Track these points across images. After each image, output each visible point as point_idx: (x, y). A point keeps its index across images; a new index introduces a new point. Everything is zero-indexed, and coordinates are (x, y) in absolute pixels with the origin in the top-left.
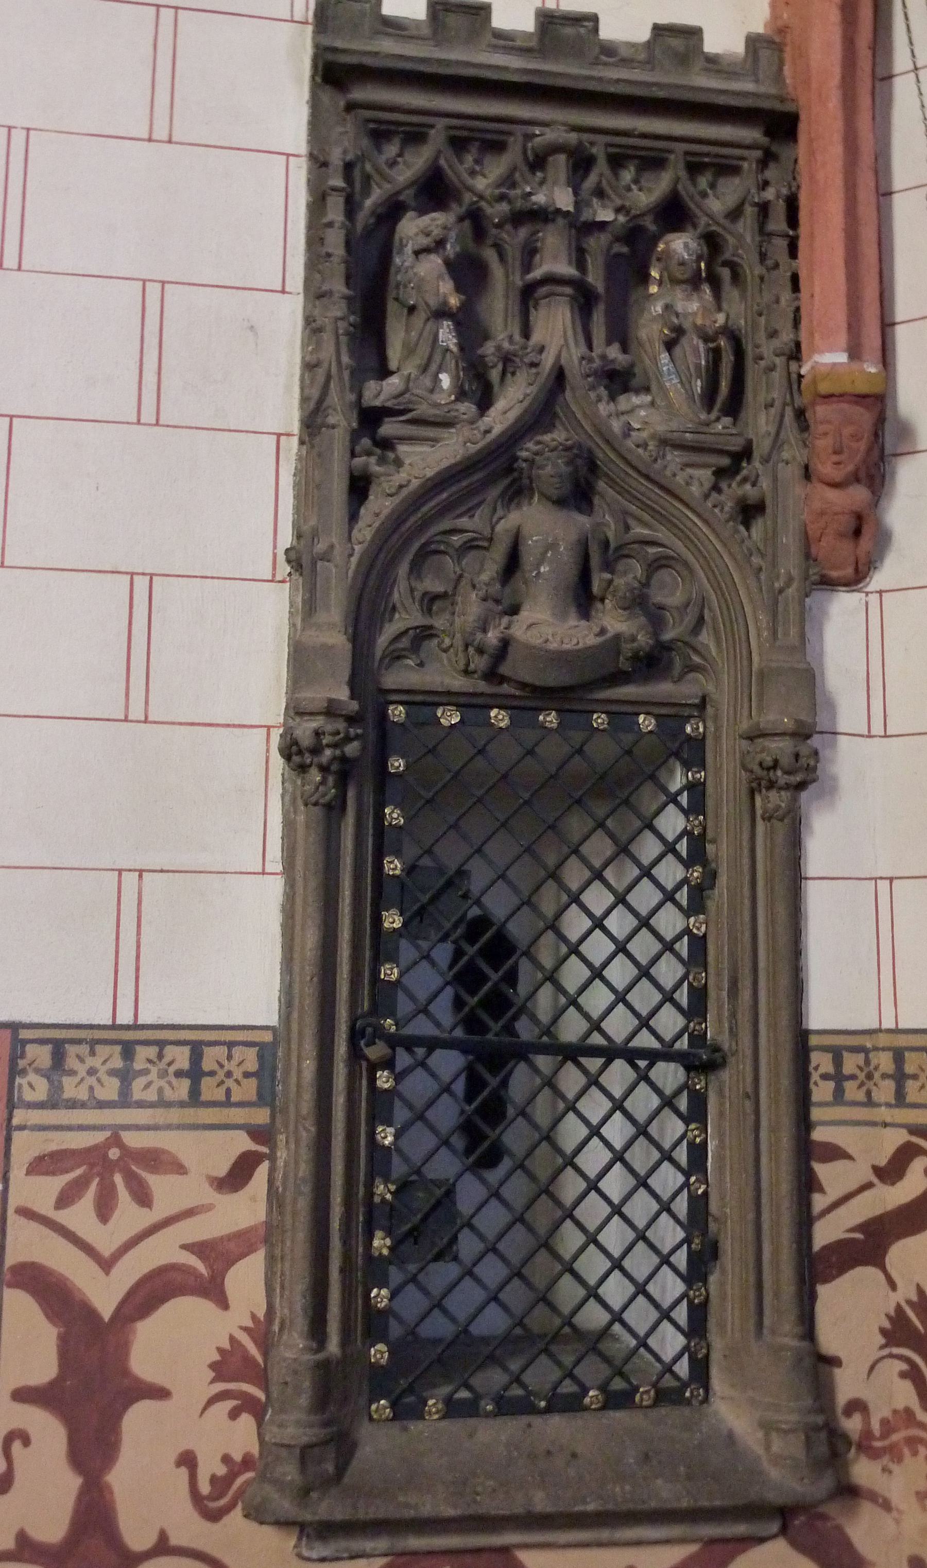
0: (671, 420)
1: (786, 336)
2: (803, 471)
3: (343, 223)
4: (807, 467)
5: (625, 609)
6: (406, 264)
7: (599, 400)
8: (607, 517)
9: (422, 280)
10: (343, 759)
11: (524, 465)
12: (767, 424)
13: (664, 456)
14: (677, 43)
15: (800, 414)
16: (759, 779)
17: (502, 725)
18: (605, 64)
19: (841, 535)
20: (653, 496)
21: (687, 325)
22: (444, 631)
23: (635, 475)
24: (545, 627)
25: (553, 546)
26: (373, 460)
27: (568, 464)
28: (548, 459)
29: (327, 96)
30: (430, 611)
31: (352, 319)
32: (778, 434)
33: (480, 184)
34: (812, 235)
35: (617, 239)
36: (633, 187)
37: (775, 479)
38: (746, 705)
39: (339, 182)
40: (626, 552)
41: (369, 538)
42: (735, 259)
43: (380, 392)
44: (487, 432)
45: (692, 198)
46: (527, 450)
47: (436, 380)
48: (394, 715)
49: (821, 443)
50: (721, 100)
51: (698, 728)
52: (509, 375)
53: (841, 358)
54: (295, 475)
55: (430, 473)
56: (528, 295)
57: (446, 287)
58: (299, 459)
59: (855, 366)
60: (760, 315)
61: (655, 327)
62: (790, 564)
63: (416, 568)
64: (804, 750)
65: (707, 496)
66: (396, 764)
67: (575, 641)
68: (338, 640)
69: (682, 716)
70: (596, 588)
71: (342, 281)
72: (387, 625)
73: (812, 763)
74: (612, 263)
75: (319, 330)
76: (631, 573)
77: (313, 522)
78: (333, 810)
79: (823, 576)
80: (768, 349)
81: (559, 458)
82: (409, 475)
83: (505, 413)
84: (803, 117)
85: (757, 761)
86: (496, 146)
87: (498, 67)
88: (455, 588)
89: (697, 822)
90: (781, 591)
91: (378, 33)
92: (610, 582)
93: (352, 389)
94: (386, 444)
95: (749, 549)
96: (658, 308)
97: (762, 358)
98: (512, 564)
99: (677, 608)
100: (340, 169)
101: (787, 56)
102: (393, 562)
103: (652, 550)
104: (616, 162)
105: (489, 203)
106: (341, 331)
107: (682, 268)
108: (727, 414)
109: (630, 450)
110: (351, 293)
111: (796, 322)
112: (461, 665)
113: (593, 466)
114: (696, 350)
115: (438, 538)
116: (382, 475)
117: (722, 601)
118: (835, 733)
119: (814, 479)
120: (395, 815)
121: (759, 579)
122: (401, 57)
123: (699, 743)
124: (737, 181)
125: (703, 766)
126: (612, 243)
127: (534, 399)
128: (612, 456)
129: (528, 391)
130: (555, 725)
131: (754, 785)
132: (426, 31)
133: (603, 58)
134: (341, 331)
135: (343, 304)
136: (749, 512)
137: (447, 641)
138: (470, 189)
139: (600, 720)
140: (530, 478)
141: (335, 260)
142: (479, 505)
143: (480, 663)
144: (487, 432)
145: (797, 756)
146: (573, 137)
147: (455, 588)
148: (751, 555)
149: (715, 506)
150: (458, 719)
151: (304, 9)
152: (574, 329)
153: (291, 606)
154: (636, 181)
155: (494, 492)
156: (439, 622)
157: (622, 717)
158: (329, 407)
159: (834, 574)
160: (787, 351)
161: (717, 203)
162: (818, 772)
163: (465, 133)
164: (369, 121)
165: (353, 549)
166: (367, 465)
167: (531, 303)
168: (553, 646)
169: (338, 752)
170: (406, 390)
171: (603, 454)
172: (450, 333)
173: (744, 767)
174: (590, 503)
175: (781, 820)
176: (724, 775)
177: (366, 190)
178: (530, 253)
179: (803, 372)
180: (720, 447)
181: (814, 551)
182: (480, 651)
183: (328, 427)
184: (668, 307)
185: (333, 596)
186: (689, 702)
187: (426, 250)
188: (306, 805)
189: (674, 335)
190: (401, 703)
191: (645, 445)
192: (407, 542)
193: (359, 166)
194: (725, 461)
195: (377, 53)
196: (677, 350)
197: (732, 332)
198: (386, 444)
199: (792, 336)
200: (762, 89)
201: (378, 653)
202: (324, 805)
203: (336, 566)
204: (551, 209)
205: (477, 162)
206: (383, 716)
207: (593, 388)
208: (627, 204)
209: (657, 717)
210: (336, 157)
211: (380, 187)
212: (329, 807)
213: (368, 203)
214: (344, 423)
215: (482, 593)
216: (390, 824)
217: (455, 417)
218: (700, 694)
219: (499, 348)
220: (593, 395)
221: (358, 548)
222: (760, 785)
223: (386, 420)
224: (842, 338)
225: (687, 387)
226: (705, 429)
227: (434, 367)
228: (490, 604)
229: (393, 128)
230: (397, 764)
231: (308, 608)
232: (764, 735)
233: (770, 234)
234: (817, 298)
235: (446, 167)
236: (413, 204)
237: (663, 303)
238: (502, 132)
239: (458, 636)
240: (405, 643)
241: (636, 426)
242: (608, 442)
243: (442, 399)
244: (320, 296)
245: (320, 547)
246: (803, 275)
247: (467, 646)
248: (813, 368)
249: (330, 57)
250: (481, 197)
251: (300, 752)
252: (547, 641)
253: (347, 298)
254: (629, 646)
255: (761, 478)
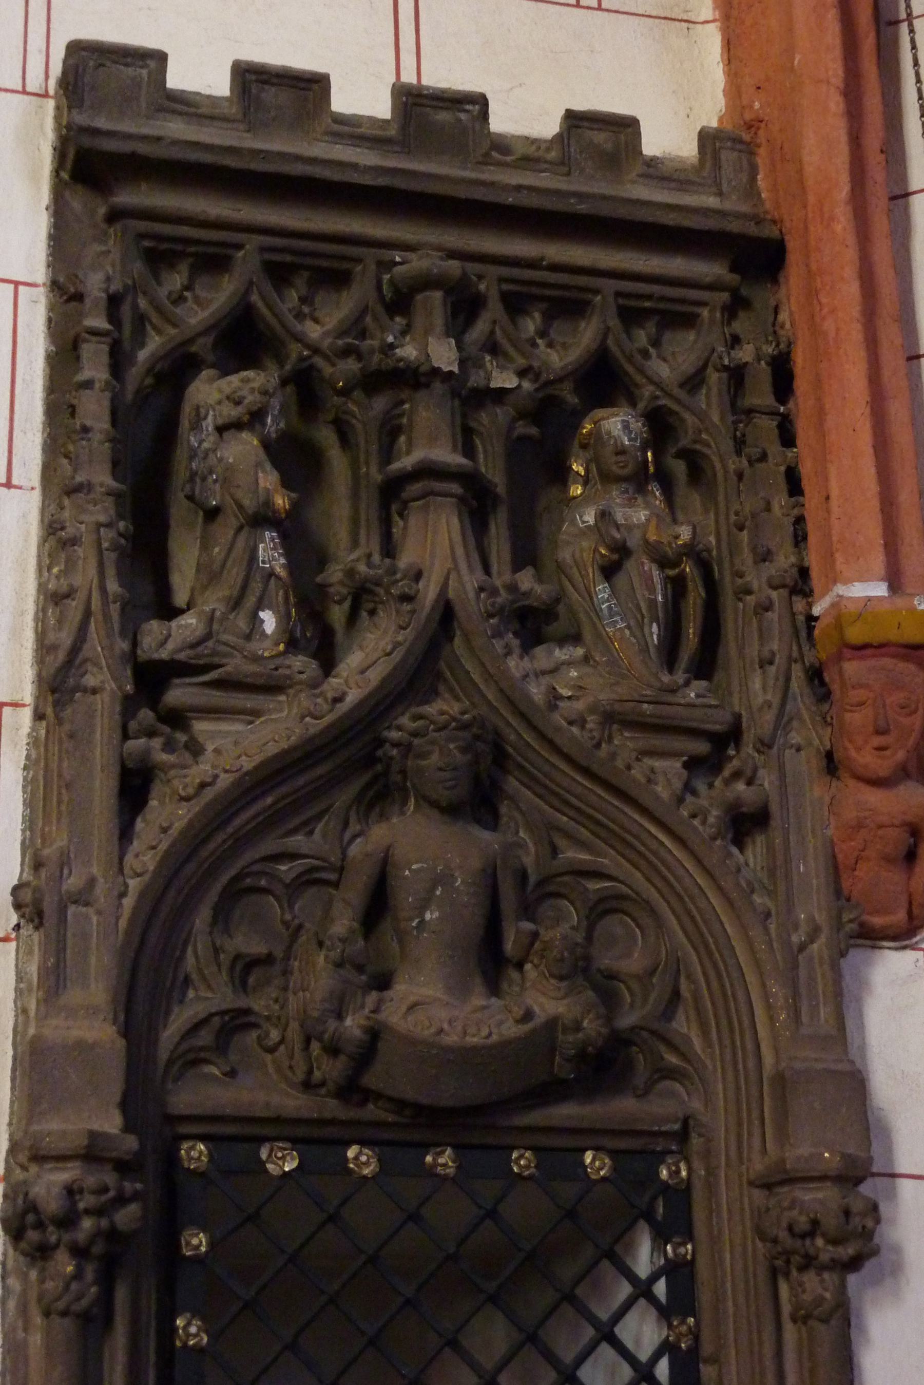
0: (617, 683)
1: (785, 560)
2: (824, 763)
3: (107, 383)
4: (829, 755)
5: (561, 978)
6: (206, 445)
7: (508, 653)
8: (522, 834)
9: (230, 468)
10: (112, 1235)
11: (395, 752)
12: (764, 688)
13: (610, 739)
14: (600, 137)
15: (815, 675)
16: (788, 1254)
17: (366, 1171)
18: (500, 164)
19: (888, 859)
20: (593, 799)
21: (633, 542)
22: (268, 1018)
23: (563, 766)
24: (432, 1006)
25: (444, 879)
26: (157, 743)
27: (464, 750)
28: (433, 743)
29: (77, 202)
30: (244, 983)
31: (122, 525)
32: (783, 704)
33: (313, 331)
34: (821, 413)
35: (522, 415)
36: (539, 341)
37: (782, 776)
38: (757, 1132)
39: (100, 322)
40: (551, 888)
41: (151, 868)
42: (698, 447)
43: (165, 639)
44: (338, 700)
45: (630, 359)
46: (399, 728)
47: (255, 621)
48: (191, 1159)
49: (856, 719)
50: (670, 219)
51: (678, 1172)
52: (364, 614)
53: (879, 590)
54: (25, 768)
55: (247, 764)
56: (393, 494)
57: (269, 479)
58: (34, 741)
59: (900, 602)
60: (741, 529)
61: (585, 544)
62: (812, 907)
63: (222, 916)
64: (857, 1206)
65: (680, 800)
66: (195, 1241)
67: (485, 1032)
68: (102, 1032)
69: (653, 1152)
70: (509, 947)
71: (108, 466)
72: (176, 1010)
73: (870, 1224)
74: (516, 449)
75: (74, 541)
76: (563, 925)
77: (61, 841)
78: (93, 1323)
79: (862, 925)
80: (756, 578)
81: (449, 740)
82: (214, 767)
83: (363, 672)
84: (793, 245)
85: (784, 1225)
86: (336, 278)
87: (341, 165)
88: (290, 947)
89: (684, 1329)
90: (802, 948)
91: (161, 109)
92: (535, 935)
93: (123, 634)
94: (177, 719)
95: (749, 883)
96: (590, 517)
97: (749, 592)
98: (378, 906)
99: (638, 977)
100: (103, 304)
101: (762, 159)
102: (184, 910)
103: (594, 885)
104: (515, 305)
105: (326, 358)
106: (105, 545)
107: (621, 458)
108: (698, 677)
109: (558, 729)
110: (122, 487)
111: (800, 538)
112: (300, 1076)
113: (500, 756)
114: (648, 581)
115: (256, 868)
116: (173, 766)
117: (708, 965)
118: (894, 1176)
119: (842, 773)
120: (193, 1330)
121: (766, 930)
122: (196, 145)
123: (680, 1196)
124: (692, 336)
125: (690, 1236)
126: (515, 420)
127: (408, 652)
128: (529, 737)
129: (400, 638)
130: (451, 1171)
131: (779, 1263)
132: (233, 110)
133: (494, 154)
134: (105, 545)
135: (109, 502)
136: (745, 823)
137: (275, 1035)
138: (298, 338)
139: (522, 1161)
140: (403, 772)
141: (97, 437)
142: (319, 817)
143: (331, 1070)
144: (338, 700)
145: (847, 1213)
146: (454, 267)
147: (290, 947)
148: (752, 892)
149: (694, 816)
150: (295, 1164)
151: (42, 76)
152: (465, 547)
153: (20, 978)
154: (543, 333)
155: (343, 797)
156: (259, 1004)
157: (558, 1157)
158: (85, 661)
159: (877, 921)
160: (789, 581)
161: (669, 363)
162: (876, 1240)
163: (288, 258)
164: (142, 236)
165: (126, 885)
166: (148, 751)
167: (394, 508)
168: (451, 1039)
169: (104, 1223)
170: (208, 636)
171: (517, 734)
172: (274, 549)
173: (761, 1234)
174: (496, 816)
175: (825, 1321)
176: (727, 1246)
177: (140, 338)
178: (391, 432)
179: (816, 611)
180: (695, 725)
181: (846, 885)
182: (333, 1050)
183: (85, 690)
184: (604, 515)
185: (93, 960)
186: (663, 1128)
187: (237, 426)
188: (47, 1314)
189: (615, 557)
190: (203, 1138)
191: (581, 722)
192: (212, 871)
193: (129, 299)
194: (702, 747)
195: (159, 139)
196: (621, 579)
197: (698, 554)
198: (177, 719)
199: (793, 559)
200: (728, 206)
201: (163, 1055)
202: (78, 1316)
203: (99, 913)
204: (423, 369)
205: (303, 300)
206: (171, 1160)
207: (498, 634)
208: (536, 364)
209: (614, 1154)
210: (95, 285)
211: (159, 332)
212: (85, 1318)
213: (143, 355)
214: (111, 685)
215: (335, 954)
216: (185, 1345)
217: (289, 677)
218: (681, 1115)
219: (350, 573)
220: (498, 646)
221: (134, 884)
222: (788, 1262)
223: (177, 681)
224: (878, 561)
225: (638, 633)
226: (670, 698)
227: (251, 601)
228: (348, 973)
229: (179, 247)
230: (197, 1241)
231: (50, 983)
232: (791, 1181)
233: (750, 412)
234: (834, 503)
235: (260, 304)
236: (211, 358)
237: (585, 512)
238: (344, 258)
239: (294, 1025)
240: (205, 1037)
241: (565, 692)
242: (523, 716)
243: (265, 649)
244: (72, 491)
245: (73, 882)
246: (806, 470)
247: (308, 1041)
248: (834, 605)
249: (87, 141)
250: (316, 351)
251: (40, 1225)
252: (441, 1031)
253: (117, 496)
254: (571, 1038)
255: (761, 772)
